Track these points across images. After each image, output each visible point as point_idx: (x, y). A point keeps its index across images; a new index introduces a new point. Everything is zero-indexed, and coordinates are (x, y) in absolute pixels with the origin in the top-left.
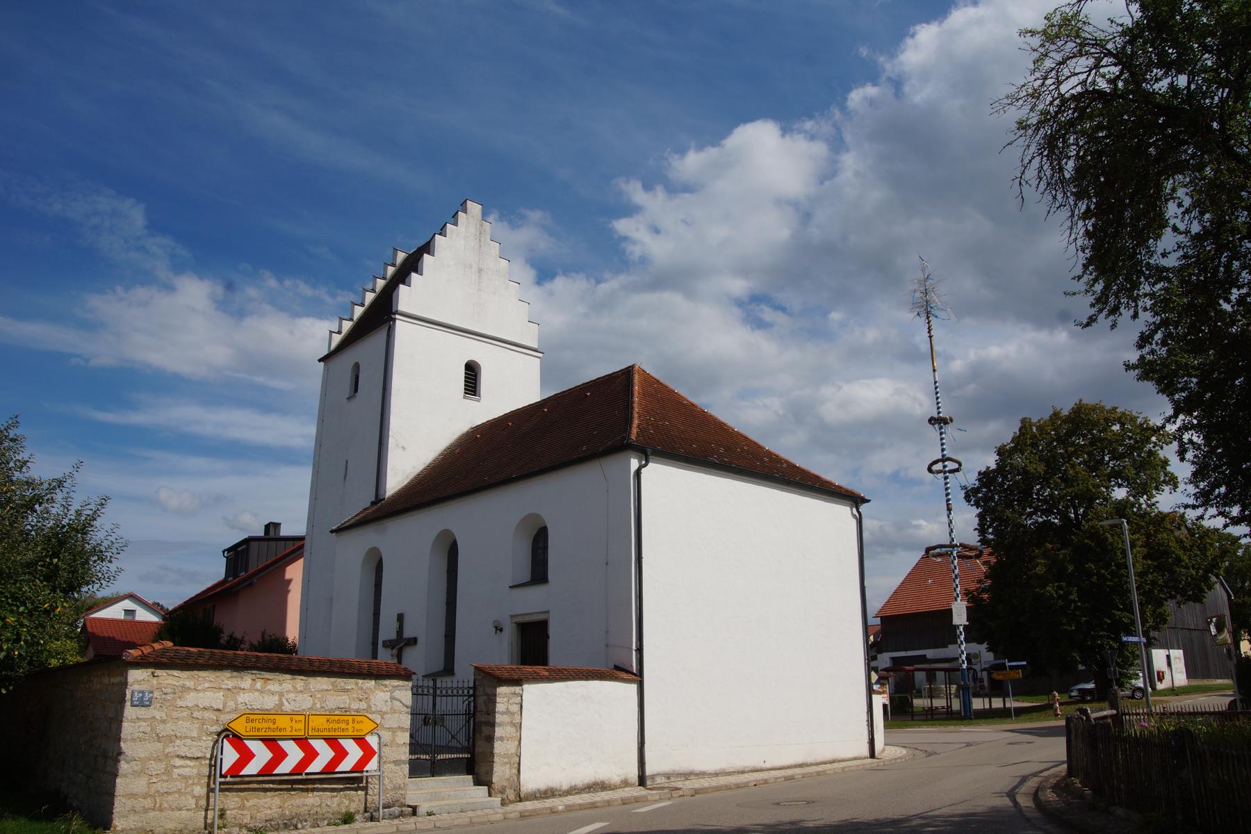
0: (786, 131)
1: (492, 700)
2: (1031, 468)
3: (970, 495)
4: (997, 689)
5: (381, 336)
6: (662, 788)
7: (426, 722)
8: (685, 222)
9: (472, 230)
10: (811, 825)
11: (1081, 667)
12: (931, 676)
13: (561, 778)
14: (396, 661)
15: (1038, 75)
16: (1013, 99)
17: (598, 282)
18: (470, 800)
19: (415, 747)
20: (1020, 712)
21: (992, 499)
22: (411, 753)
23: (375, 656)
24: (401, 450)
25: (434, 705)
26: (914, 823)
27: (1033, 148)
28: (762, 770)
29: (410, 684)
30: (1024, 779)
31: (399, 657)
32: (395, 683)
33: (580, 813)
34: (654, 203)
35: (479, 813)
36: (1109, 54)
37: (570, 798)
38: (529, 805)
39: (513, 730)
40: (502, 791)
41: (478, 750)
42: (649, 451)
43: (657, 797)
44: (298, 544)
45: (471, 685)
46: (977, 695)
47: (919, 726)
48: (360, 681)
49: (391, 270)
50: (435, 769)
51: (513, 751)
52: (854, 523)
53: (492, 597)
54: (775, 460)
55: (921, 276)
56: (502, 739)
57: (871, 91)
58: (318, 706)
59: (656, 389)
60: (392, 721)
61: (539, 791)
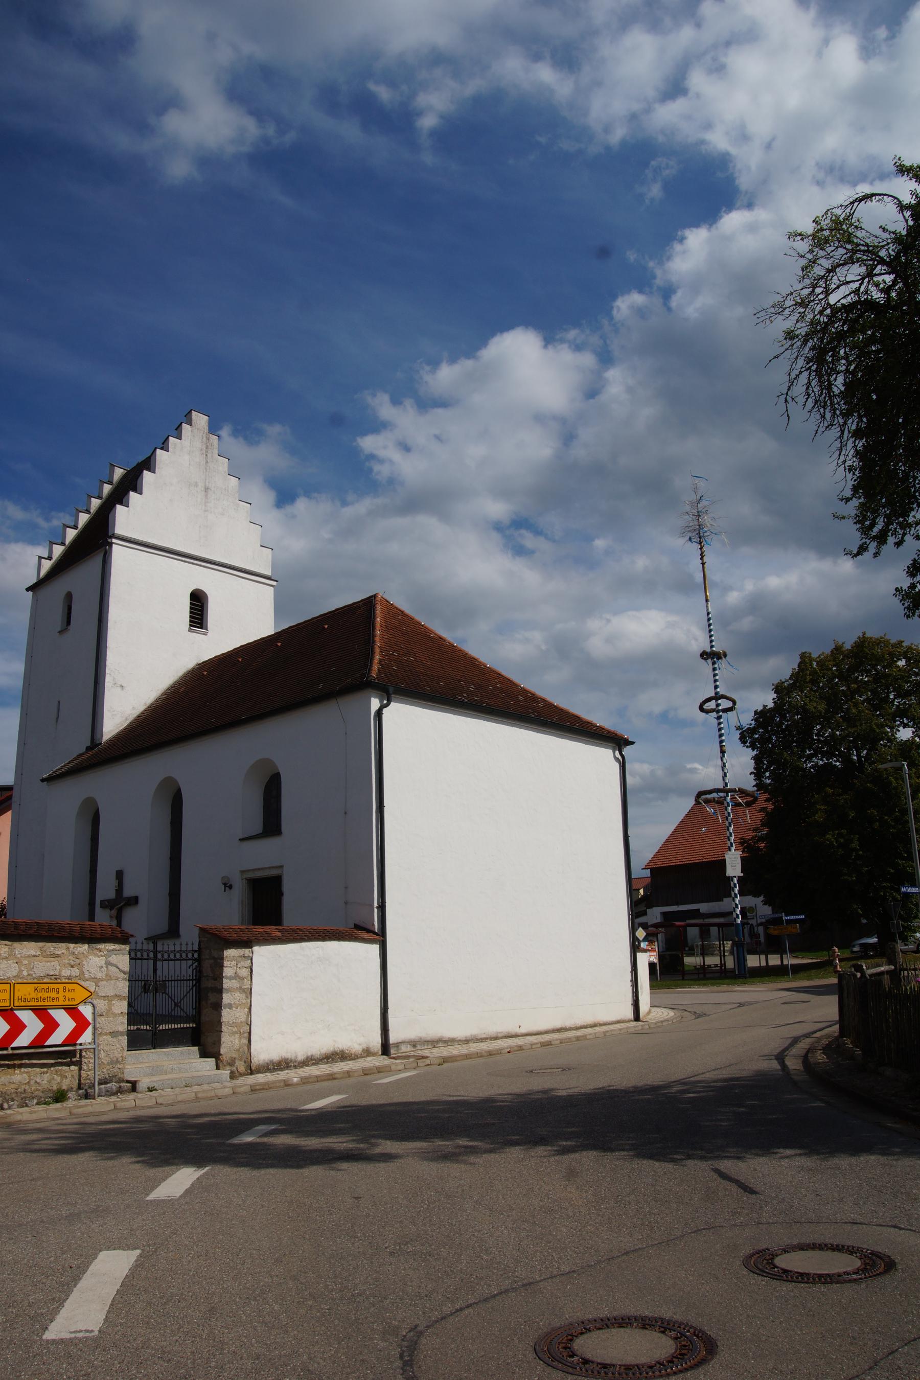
0: (549, 341)
1: (219, 965)
2: (810, 707)
3: (745, 736)
4: (774, 945)
5: (96, 562)
6: (408, 1057)
7: (146, 989)
8: (438, 438)
9: (198, 444)
10: (564, 1093)
11: (864, 921)
12: (705, 932)
13: (298, 1049)
14: (114, 923)
15: (807, 282)
16: (780, 308)
17: (345, 503)
18: (195, 1074)
19: (133, 1016)
20: (797, 970)
21: (770, 739)
22: (129, 1024)
23: (92, 917)
24: (119, 689)
25: (155, 970)
26: (674, 1089)
27: (801, 362)
28: (516, 1036)
29: (128, 948)
30: (795, 1040)
31: (119, 918)
32: (111, 946)
33: (317, 1085)
34: (406, 420)
35: (206, 1087)
36: (882, 261)
37: (307, 1069)
38: (261, 1078)
39: (243, 996)
40: (232, 1063)
41: (204, 1018)
42: (391, 689)
43: (401, 1067)
44: (8, 794)
45: (196, 947)
46: (752, 952)
47: (690, 986)
48: (72, 946)
49: (107, 488)
50: (157, 1041)
51: (243, 1018)
52: (616, 766)
53: (219, 852)
54: (531, 698)
55: (694, 498)
56: (230, 1006)
57: (637, 298)
58: (25, 973)
59: (402, 623)
60: (107, 989)
61: (272, 1062)
